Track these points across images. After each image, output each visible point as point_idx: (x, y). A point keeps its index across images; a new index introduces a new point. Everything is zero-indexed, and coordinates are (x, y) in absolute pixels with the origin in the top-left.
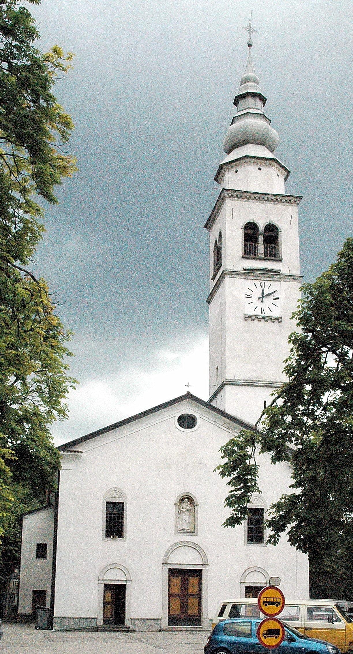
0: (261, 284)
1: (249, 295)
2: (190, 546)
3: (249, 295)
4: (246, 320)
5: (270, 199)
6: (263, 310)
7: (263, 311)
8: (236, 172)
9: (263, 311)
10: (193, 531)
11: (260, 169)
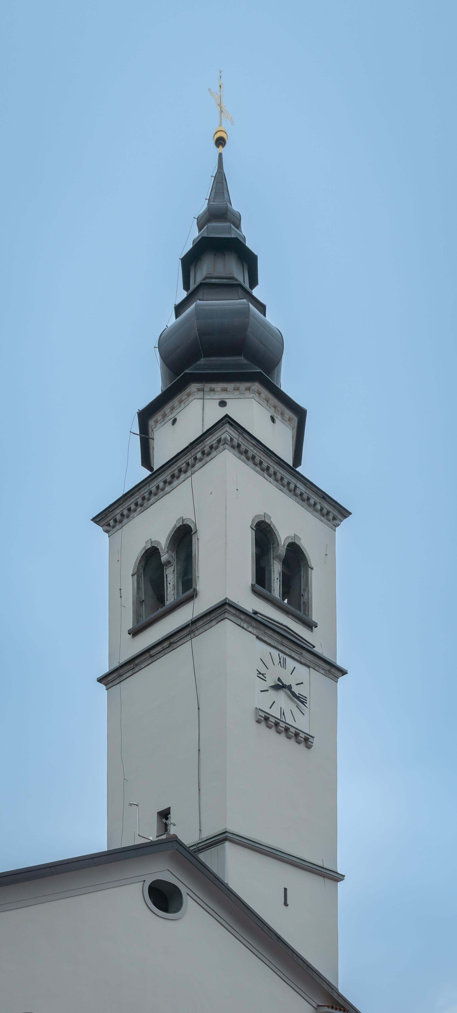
1: (263, 675)
3: (263, 675)
4: (258, 722)
5: (298, 492)
6: (284, 714)
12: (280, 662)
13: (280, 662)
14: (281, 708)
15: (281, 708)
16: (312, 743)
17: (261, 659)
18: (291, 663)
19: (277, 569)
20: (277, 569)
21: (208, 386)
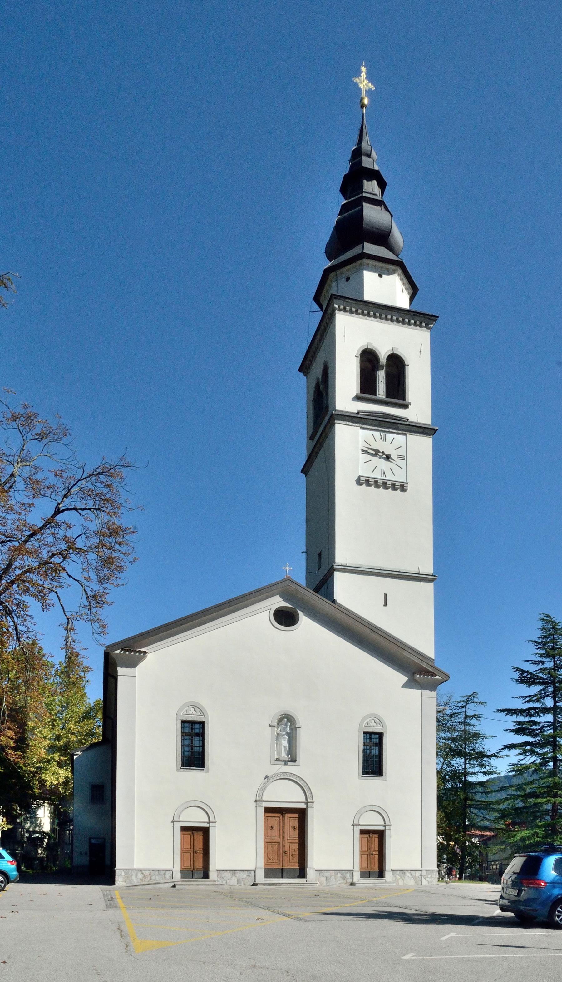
0: (381, 436)
2: (291, 778)
6: (384, 473)
7: (383, 473)
9: (383, 473)
12: (381, 438)
13: (381, 438)
14: (382, 469)
15: (382, 469)
16: (407, 487)
17: (365, 441)
18: (390, 436)
19: (381, 375)
20: (381, 375)
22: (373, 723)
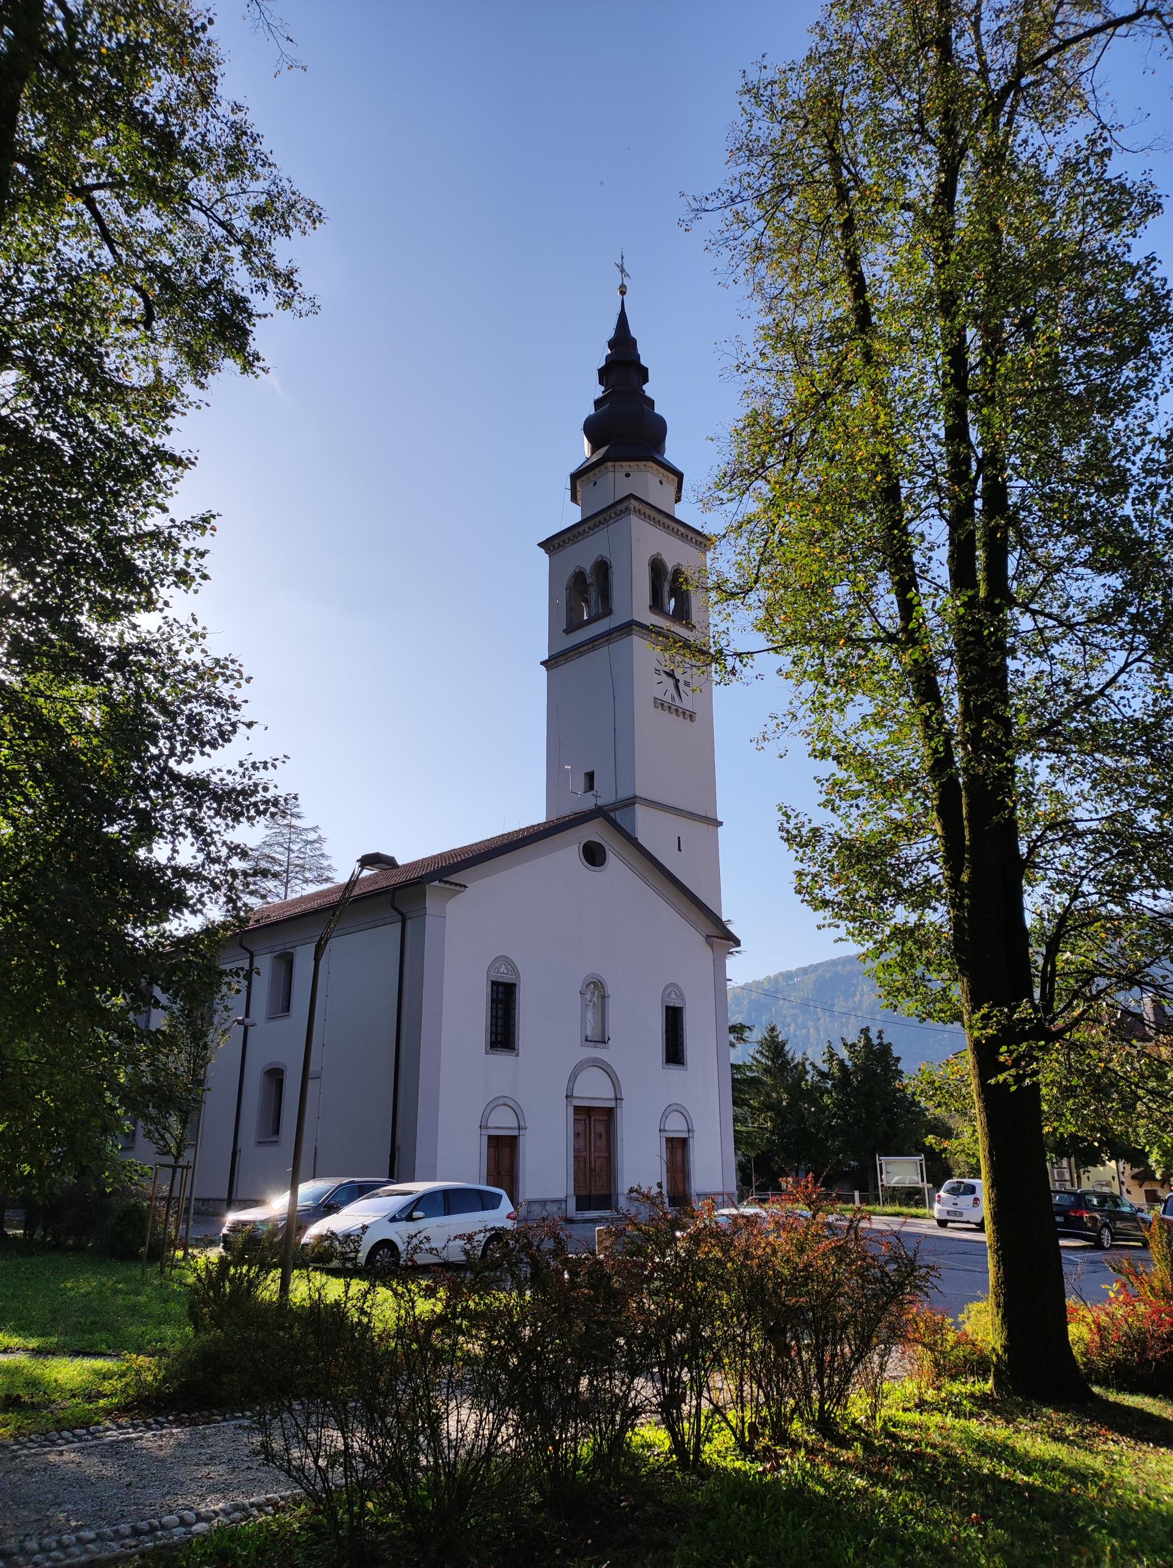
8: (628, 475)
10: (603, 1041)
11: (661, 483)
21: (617, 464)
22: (503, 969)
